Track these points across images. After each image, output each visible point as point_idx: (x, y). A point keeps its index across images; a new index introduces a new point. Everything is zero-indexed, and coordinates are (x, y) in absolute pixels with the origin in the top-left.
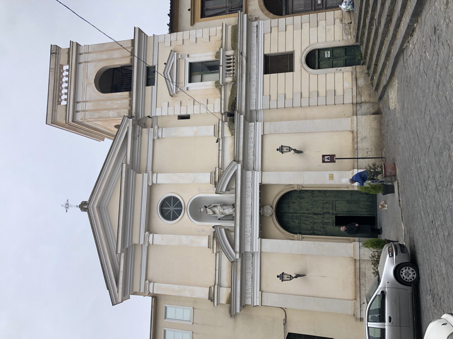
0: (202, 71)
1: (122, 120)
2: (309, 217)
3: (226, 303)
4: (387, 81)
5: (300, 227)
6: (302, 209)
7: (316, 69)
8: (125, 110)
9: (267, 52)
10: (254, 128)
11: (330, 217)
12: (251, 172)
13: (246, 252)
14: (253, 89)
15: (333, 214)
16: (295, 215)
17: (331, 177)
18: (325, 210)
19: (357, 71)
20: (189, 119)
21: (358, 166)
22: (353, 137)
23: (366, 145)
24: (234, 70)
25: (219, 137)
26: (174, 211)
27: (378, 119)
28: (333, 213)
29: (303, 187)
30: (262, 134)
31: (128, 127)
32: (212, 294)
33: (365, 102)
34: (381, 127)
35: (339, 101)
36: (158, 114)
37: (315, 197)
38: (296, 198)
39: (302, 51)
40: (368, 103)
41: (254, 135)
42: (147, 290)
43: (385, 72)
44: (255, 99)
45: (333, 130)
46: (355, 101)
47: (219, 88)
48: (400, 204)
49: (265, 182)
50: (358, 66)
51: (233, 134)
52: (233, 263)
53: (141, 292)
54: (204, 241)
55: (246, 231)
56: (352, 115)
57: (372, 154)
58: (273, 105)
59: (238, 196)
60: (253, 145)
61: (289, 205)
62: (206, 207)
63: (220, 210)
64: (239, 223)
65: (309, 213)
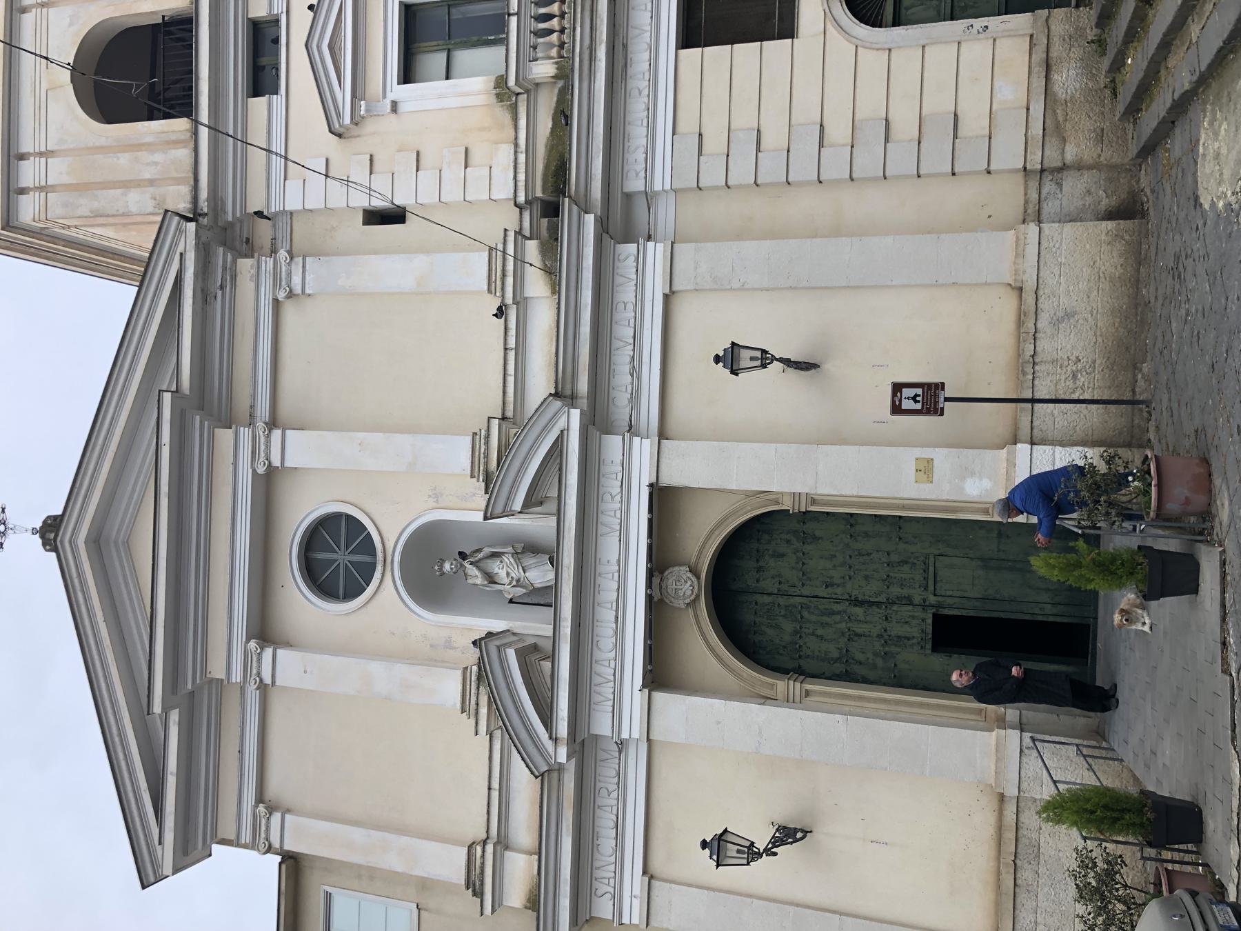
0: (449, 39)
1: (160, 229)
2: (833, 613)
4: (1195, 78)
5: (800, 646)
6: (810, 579)
7: (886, 27)
8: (180, 187)
10: (635, 264)
11: (913, 617)
12: (621, 437)
14: (637, 108)
15: (924, 606)
16: (782, 601)
17: (925, 469)
18: (896, 591)
19: (1052, 34)
20: (404, 222)
21: (1035, 431)
23: (1069, 347)
24: (562, 31)
25: (503, 300)
26: (350, 566)
27: (1127, 237)
28: (924, 601)
29: (814, 502)
30: (667, 291)
31: (181, 254)
32: (478, 871)
33: (1079, 167)
34: (1138, 271)
35: (972, 159)
36: (293, 204)
37: (860, 538)
38: (788, 537)
40: (1090, 167)
41: (636, 296)
42: (263, 835)
43: (1194, 30)
44: (643, 150)
45: (940, 281)
46: (1035, 163)
47: (511, 105)
48: (1225, 661)
49: (668, 480)
50: (1059, 13)
51: (555, 289)
52: (547, 776)
53: (243, 842)
54: (449, 687)
55: (596, 662)
56: (1021, 218)
57: (1091, 385)
58: (713, 175)
59: (569, 529)
60: (632, 334)
61: (761, 564)
62: (463, 555)
63: (509, 571)
64: (568, 631)
65: (834, 596)
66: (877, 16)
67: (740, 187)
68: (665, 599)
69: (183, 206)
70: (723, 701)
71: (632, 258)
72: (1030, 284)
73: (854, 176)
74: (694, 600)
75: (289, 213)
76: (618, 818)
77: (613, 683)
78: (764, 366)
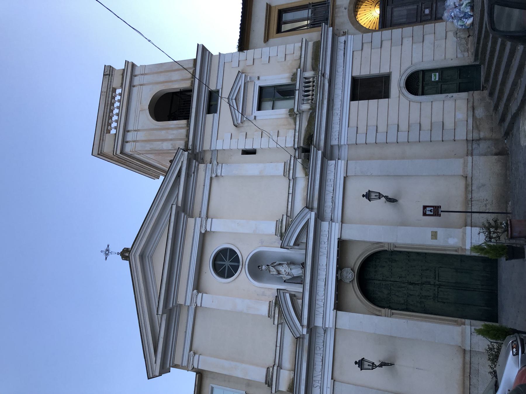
0: (274, 97)
3: (287, 391)
9: (356, 74)
10: (334, 167)
11: (431, 289)
12: (328, 223)
13: (316, 327)
14: (336, 119)
16: (384, 283)
17: (434, 235)
18: (424, 279)
22: (466, 184)
24: (313, 95)
26: (230, 266)
29: (396, 247)
30: (345, 176)
31: (182, 161)
33: (485, 139)
36: (219, 147)
39: (401, 73)
44: (338, 132)
46: (470, 137)
49: (345, 237)
50: (476, 92)
51: (307, 174)
53: (184, 365)
54: (264, 309)
59: (310, 252)
60: (333, 189)
63: (285, 269)
65: (402, 281)
66: (416, 93)
67: (370, 144)
68: (342, 279)
69: (182, 147)
70: (363, 315)
71: (333, 165)
72: (470, 175)
73: (409, 141)
74: (352, 281)
75: (217, 150)
76: (323, 358)
77: (323, 308)
78: (380, 198)
